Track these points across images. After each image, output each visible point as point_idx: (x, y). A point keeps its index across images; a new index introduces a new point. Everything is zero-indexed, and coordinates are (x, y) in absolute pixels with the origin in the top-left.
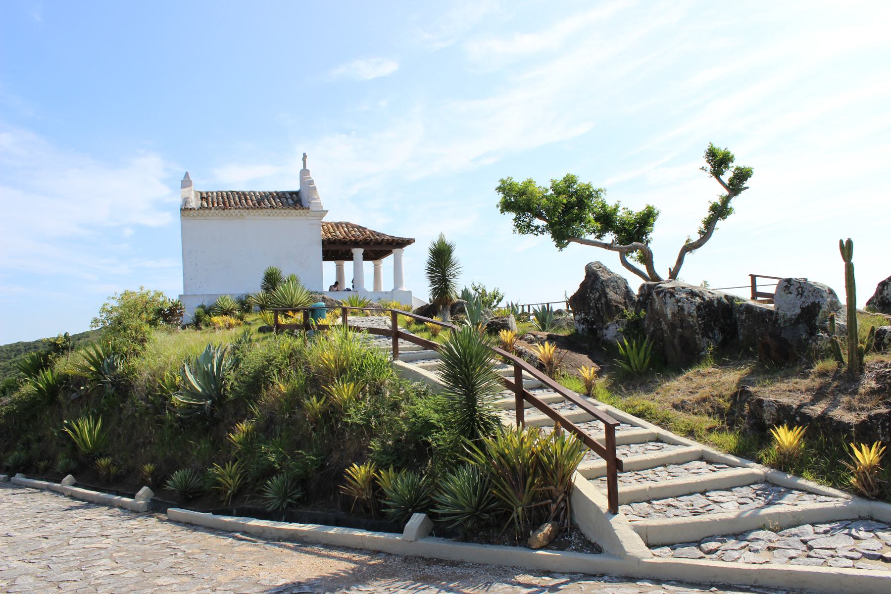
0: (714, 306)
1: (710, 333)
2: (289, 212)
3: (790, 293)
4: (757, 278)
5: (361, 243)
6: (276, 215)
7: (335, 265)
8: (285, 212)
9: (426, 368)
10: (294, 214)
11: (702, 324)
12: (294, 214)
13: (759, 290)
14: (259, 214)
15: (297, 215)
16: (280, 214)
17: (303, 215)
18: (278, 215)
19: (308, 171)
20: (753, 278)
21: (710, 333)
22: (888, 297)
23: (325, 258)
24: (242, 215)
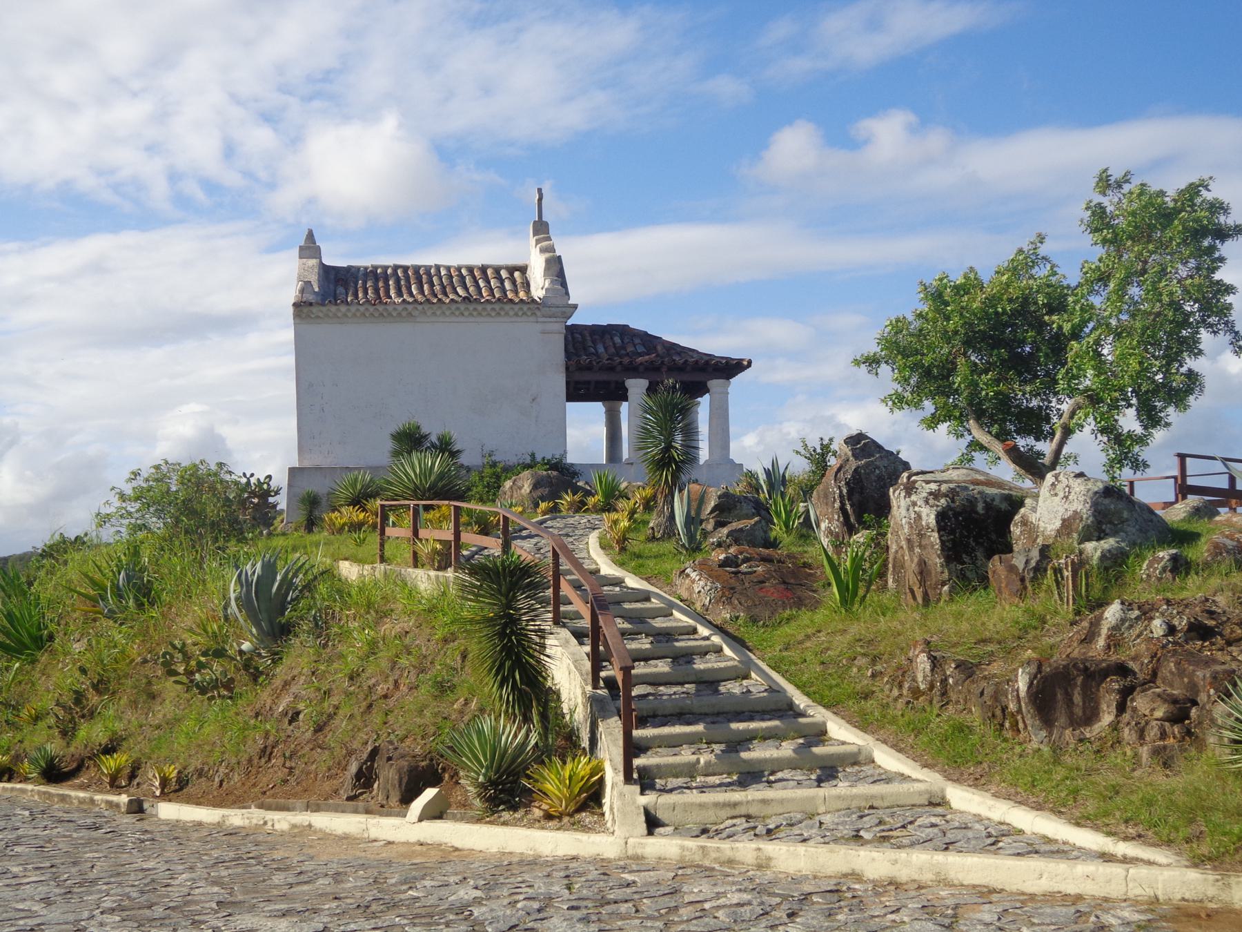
0: (977, 513)
1: (964, 556)
2: (502, 309)
3: (1056, 495)
4: (1188, 460)
5: (641, 369)
6: (475, 313)
7: (603, 409)
8: (493, 309)
9: (904, 778)
10: (511, 313)
11: (948, 541)
12: (511, 313)
13: (1190, 481)
14: (444, 313)
15: (516, 315)
16: (484, 313)
17: (529, 314)
18: (480, 314)
19: (547, 224)
20: (1182, 457)
21: (964, 556)
22: (85, 539)
23: (577, 392)
24: (410, 314)
